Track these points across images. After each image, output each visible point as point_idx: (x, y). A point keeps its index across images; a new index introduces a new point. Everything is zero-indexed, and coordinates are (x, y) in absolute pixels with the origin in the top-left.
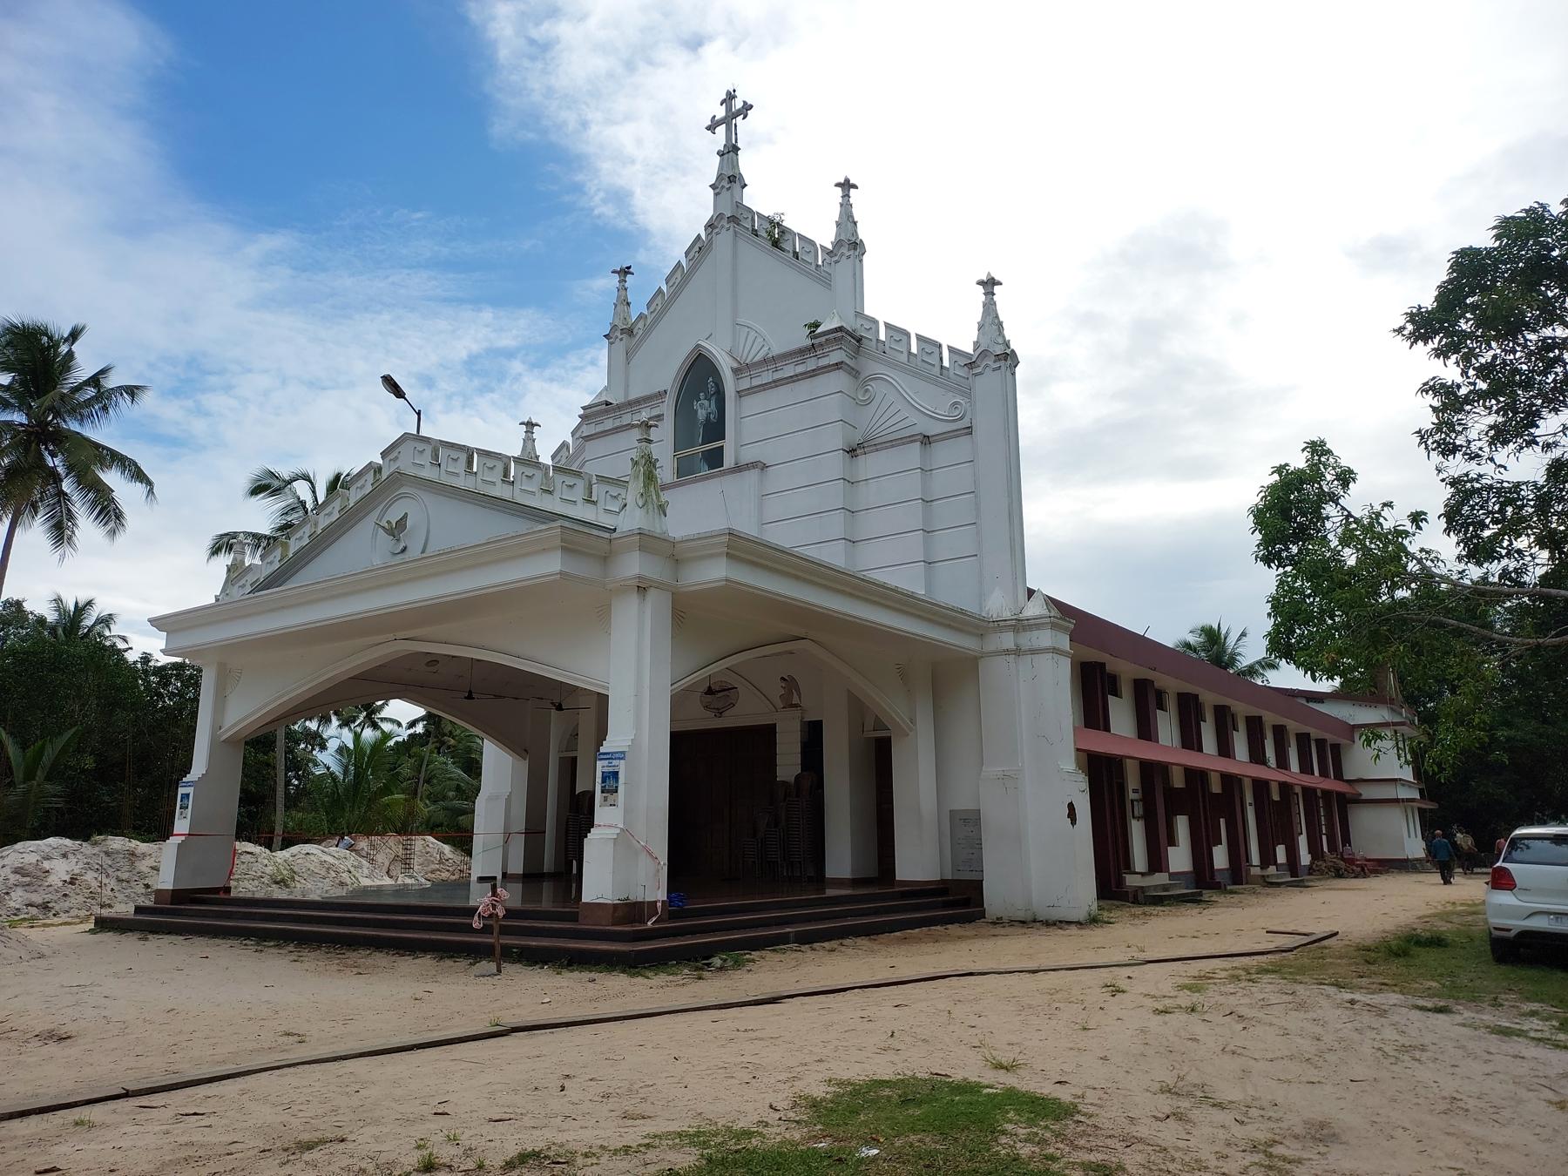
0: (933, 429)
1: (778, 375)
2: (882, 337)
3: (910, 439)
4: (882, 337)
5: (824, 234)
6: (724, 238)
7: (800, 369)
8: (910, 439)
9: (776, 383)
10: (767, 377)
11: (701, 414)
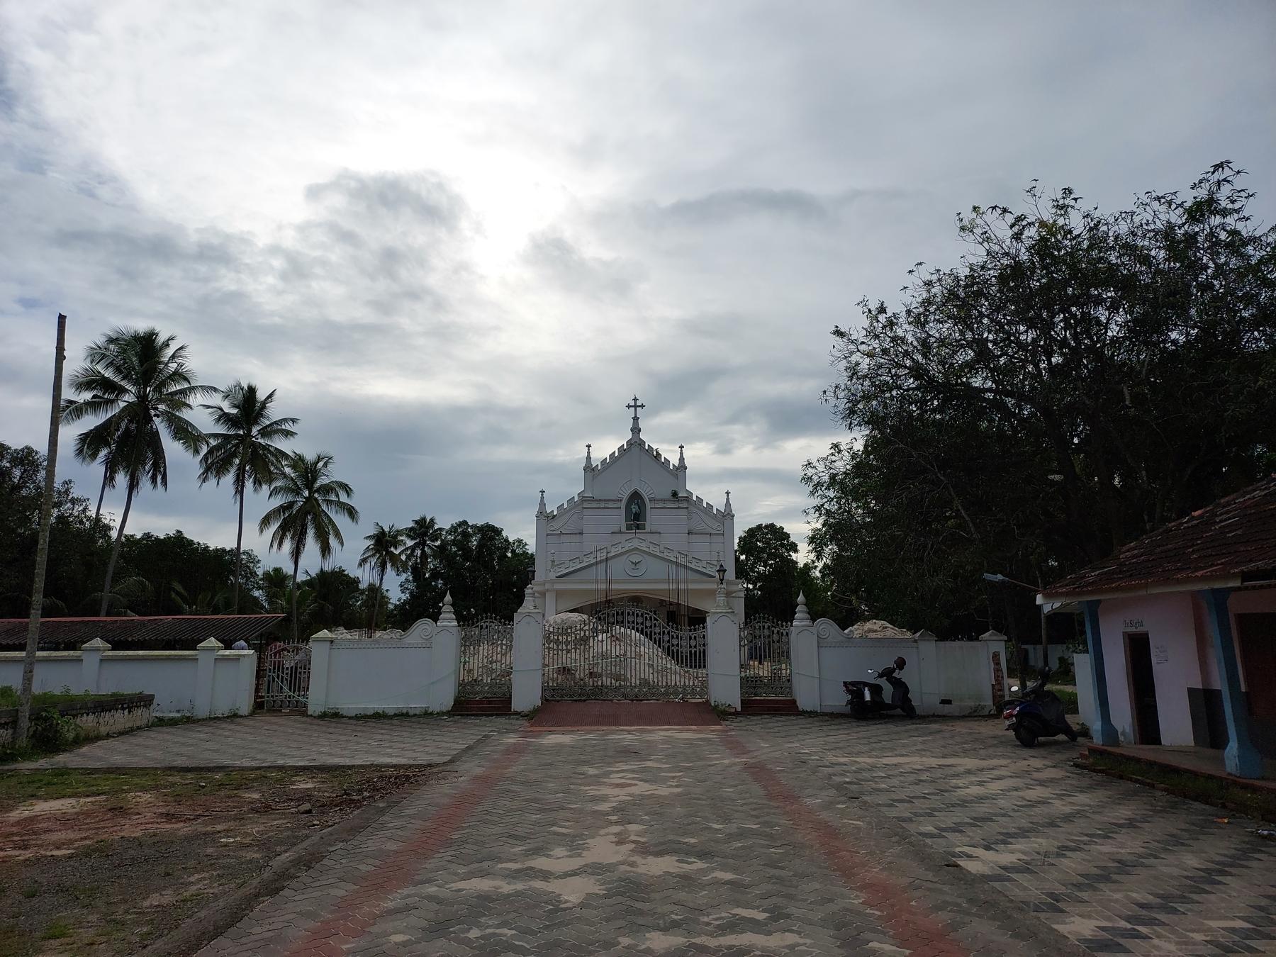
1: (665, 505)
2: (671, 467)
3: (707, 534)
5: (674, 460)
6: (635, 450)
7: (672, 506)
8: (707, 534)
10: (661, 505)
11: (634, 510)
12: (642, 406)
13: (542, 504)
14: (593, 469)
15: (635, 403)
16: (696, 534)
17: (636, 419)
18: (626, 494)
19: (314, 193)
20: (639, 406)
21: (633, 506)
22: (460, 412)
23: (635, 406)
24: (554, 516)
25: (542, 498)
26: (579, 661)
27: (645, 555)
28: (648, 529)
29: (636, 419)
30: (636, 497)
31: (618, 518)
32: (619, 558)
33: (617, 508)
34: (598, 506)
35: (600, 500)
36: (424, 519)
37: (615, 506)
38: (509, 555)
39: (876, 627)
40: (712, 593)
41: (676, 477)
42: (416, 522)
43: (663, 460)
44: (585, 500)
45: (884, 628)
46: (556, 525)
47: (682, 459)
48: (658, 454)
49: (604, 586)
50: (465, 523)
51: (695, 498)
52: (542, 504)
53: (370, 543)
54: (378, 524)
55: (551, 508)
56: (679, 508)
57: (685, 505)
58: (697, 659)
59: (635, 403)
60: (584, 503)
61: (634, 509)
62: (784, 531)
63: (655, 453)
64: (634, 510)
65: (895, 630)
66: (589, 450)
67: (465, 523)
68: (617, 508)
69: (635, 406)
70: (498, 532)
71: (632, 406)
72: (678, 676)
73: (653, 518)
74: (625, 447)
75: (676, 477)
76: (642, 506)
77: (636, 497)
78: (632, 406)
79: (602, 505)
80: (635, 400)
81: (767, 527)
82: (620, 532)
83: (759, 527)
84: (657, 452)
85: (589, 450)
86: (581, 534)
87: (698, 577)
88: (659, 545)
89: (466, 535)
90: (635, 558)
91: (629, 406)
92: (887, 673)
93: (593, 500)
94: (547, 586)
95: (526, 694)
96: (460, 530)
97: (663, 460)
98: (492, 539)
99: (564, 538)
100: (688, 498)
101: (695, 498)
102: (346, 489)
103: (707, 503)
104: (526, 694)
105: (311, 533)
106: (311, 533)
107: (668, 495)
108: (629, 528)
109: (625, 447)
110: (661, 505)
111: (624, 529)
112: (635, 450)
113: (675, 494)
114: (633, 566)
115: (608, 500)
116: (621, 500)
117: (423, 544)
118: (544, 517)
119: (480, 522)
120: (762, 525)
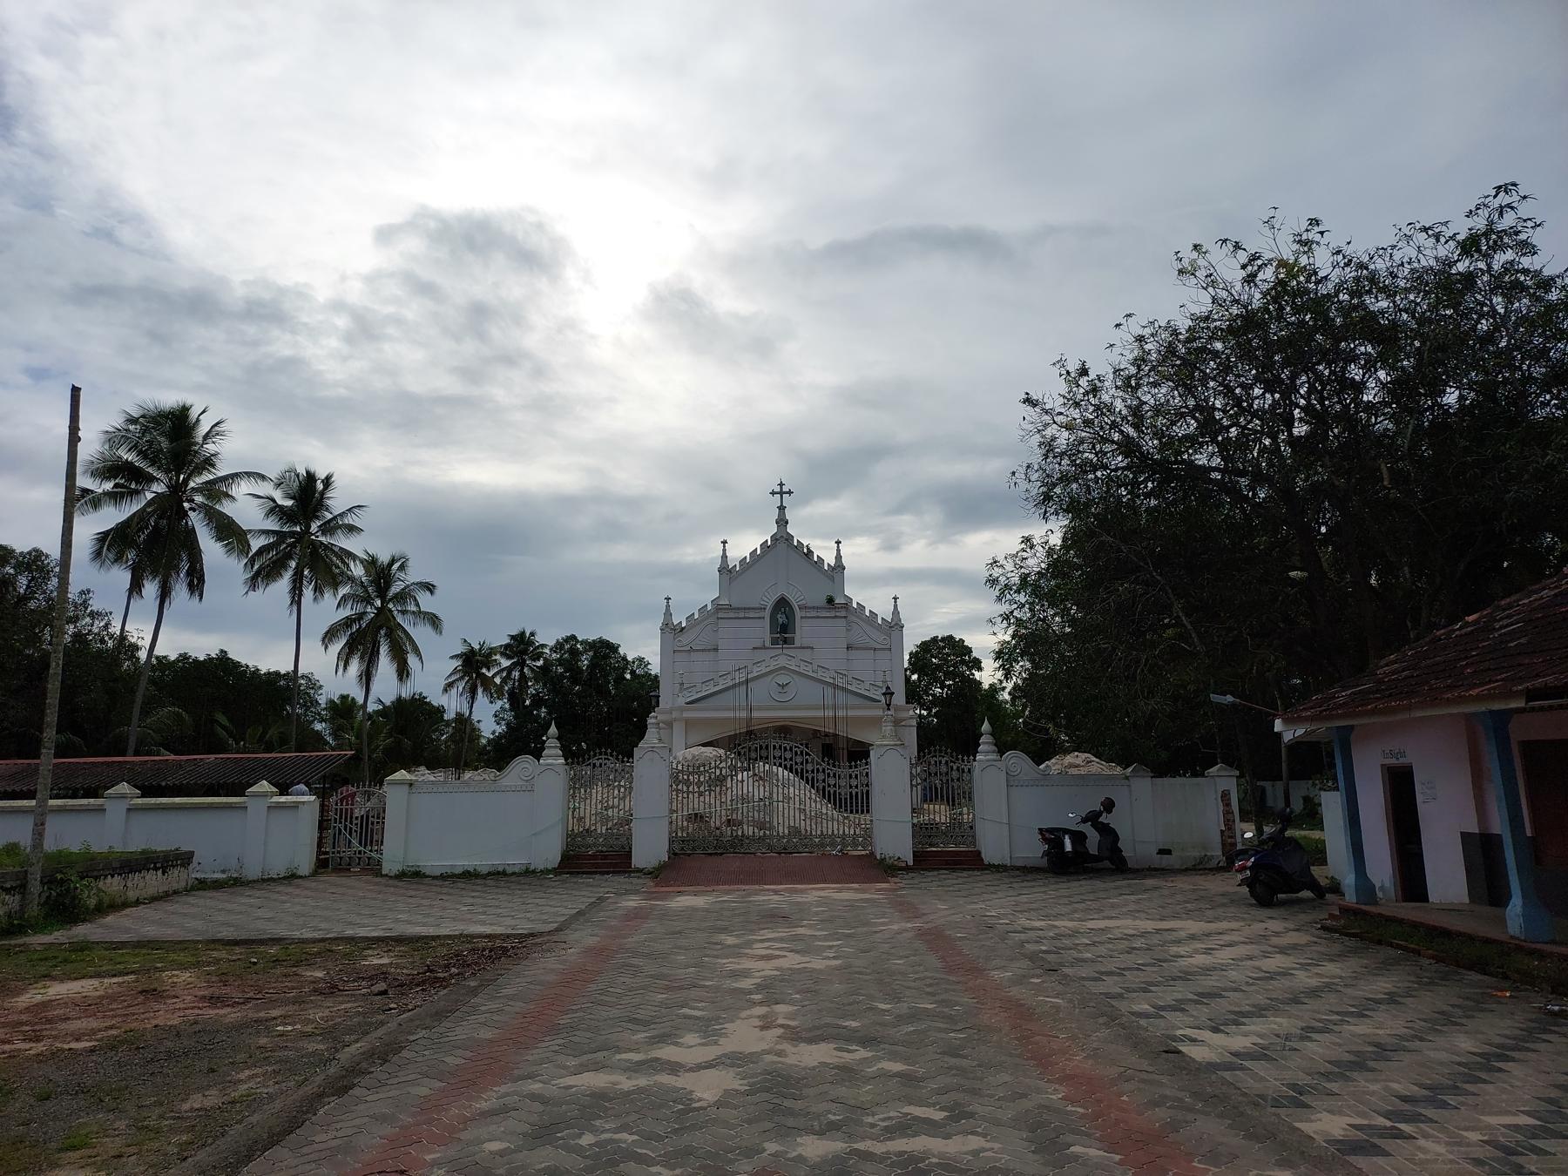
0: (878, 646)
3: (871, 649)
4: (826, 568)
5: (830, 559)
6: (782, 546)
7: (828, 614)
8: (871, 649)
9: (818, 617)
11: (780, 621)
12: (790, 493)
13: (668, 614)
14: (730, 571)
15: (781, 488)
16: (857, 649)
17: (782, 508)
18: (770, 603)
19: (385, 235)
20: (786, 493)
21: (779, 616)
22: (568, 503)
23: (781, 493)
24: (683, 629)
25: (668, 606)
26: (714, 806)
27: (794, 676)
28: (797, 643)
29: (782, 508)
30: (782, 604)
31: (761, 630)
32: (762, 680)
33: (760, 618)
34: (736, 615)
35: (738, 609)
37: (757, 615)
39: (1078, 761)
41: (832, 579)
42: (512, 637)
43: (816, 559)
44: (721, 609)
45: (1088, 762)
46: (685, 639)
47: (839, 557)
48: (810, 552)
49: (744, 714)
51: (855, 605)
52: (668, 614)
53: (457, 663)
54: (465, 641)
55: (679, 618)
56: (836, 617)
57: (843, 614)
58: (858, 802)
59: (781, 488)
60: (718, 612)
61: (781, 619)
63: (805, 550)
64: (780, 621)
65: (1102, 764)
66: (724, 546)
67: (573, 637)
68: (760, 618)
69: (781, 493)
70: (613, 648)
71: (777, 493)
72: (835, 823)
73: (804, 630)
74: (769, 544)
75: (832, 579)
76: (790, 615)
77: (782, 604)
78: (777, 493)
79: (741, 615)
80: (781, 485)
81: (943, 639)
82: (764, 648)
83: (935, 639)
84: (808, 549)
85: (724, 546)
86: (716, 650)
87: (859, 701)
88: (811, 663)
89: (574, 653)
90: (783, 680)
91: (773, 493)
92: (1092, 818)
93: (730, 608)
95: (649, 847)
96: (567, 647)
97: (816, 559)
98: (606, 657)
100: (847, 605)
101: (855, 605)
103: (858, 603)
104: (649, 847)
105: (384, 650)
106: (384, 650)
107: (822, 601)
108: (774, 642)
109: (769, 544)
110: (814, 614)
111: (768, 644)
112: (782, 546)
113: (830, 600)
114: (780, 689)
115: (749, 609)
116: (765, 609)
117: (522, 664)
118: (670, 630)
119: (592, 637)
120: (937, 637)
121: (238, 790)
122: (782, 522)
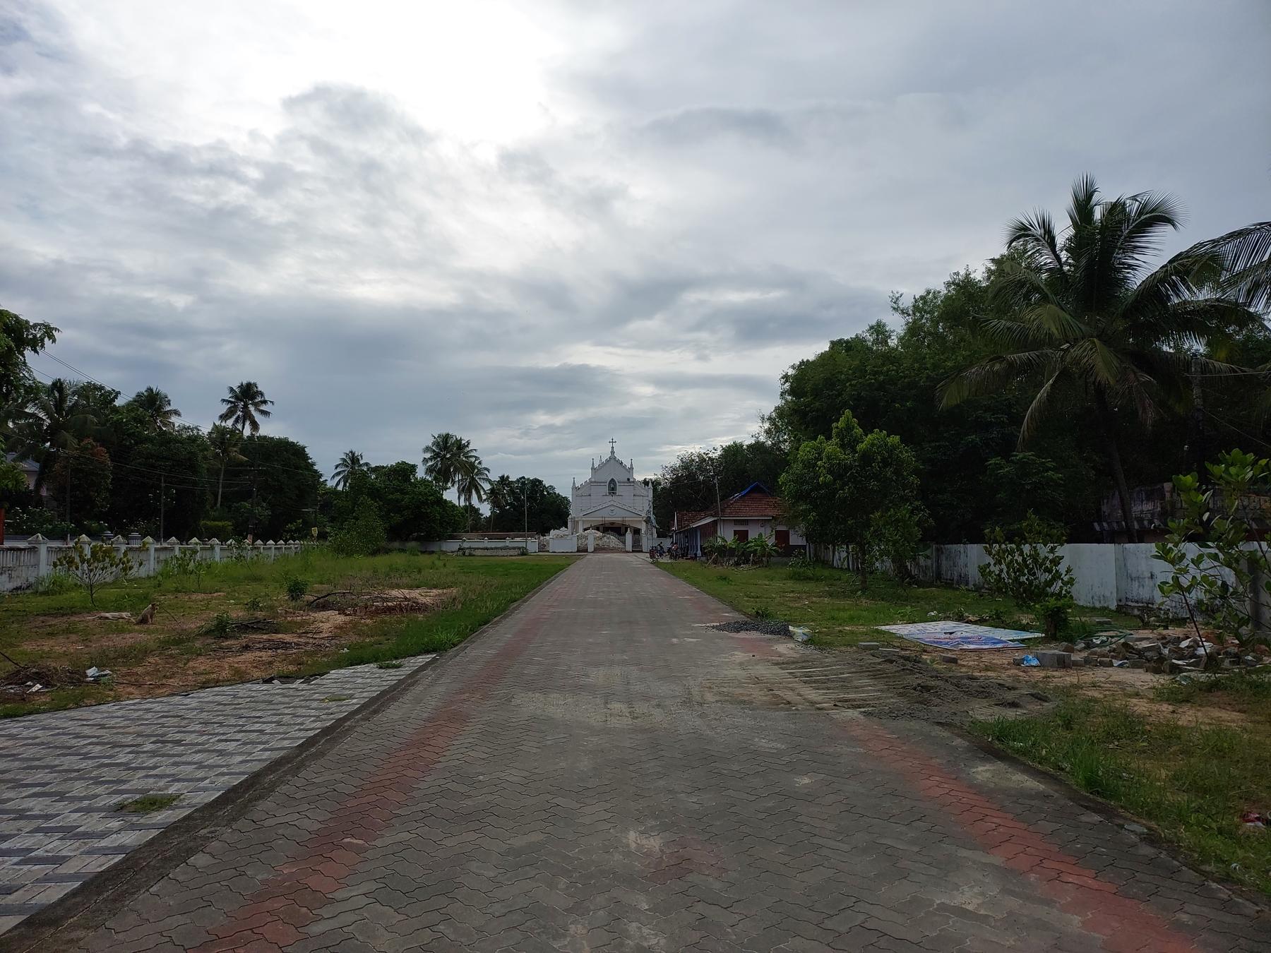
6: (612, 461)
17: (613, 447)
19: (292, 104)
22: (442, 316)
26: (600, 543)
29: (613, 447)
31: (606, 490)
36: (503, 476)
38: (546, 493)
40: (640, 521)
46: (580, 492)
47: (632, 465)
50: (523, 477)
58: (624, 543)
60: (591, 483)
61: (612, 486)
62: (979, 275)
70: (540, 482)
72: (621, 545)
73: (619, 489)
76: (615, 485)
86: (590, 495)
87: (635, 515)
92: (659, 545)
93: (595, 482)
94: (580, 519)
95: (591, 549)
96: (521, 481)
99: (583, 498)
102: (488, 470)
104: (591, 549)
105: (474, 492)
106: (474, 492)
108: (610, 493)
112: (612, 461)
113: (628, 479)
118: (575, 488)
121: (505, 539)
122: (613, 452)
